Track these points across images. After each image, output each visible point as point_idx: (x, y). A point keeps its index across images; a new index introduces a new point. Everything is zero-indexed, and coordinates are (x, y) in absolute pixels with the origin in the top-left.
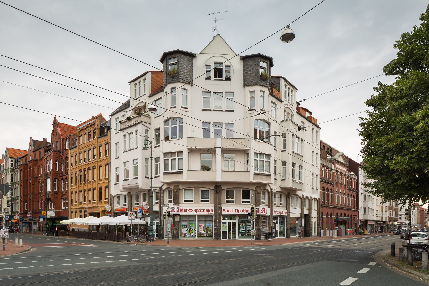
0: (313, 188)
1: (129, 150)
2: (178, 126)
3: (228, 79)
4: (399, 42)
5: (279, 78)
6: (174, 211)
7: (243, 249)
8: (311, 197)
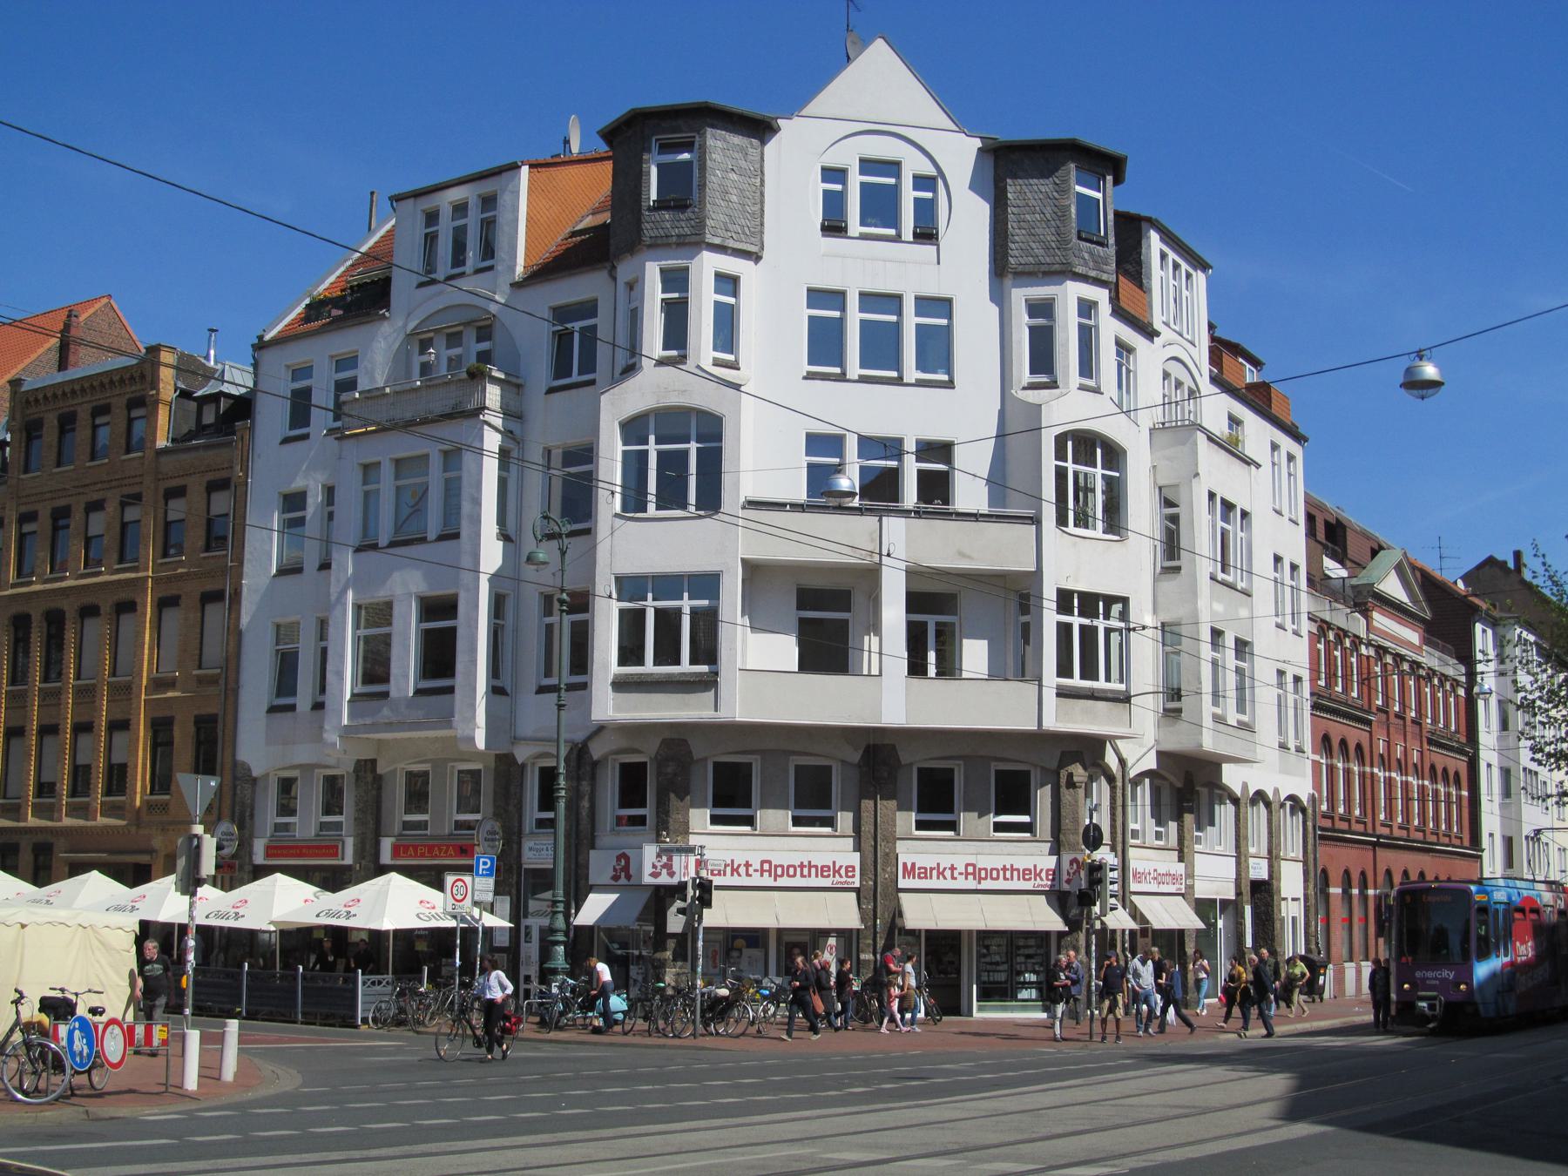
6: (671, 874)
8: (1276, 791)
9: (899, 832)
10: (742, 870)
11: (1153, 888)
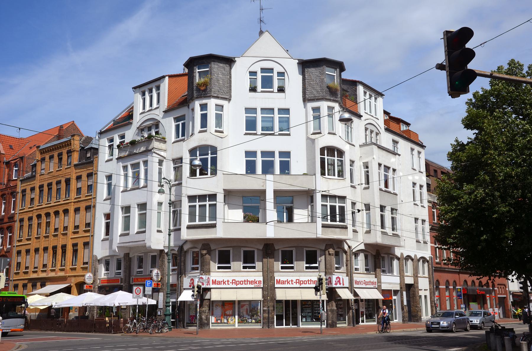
0: (418, 241)
1: (131, 190)
2: (209, 156)
3: (281, 90)
4: (471, 100)
5: (354, 83)
7: (308, 339)
9: (275, 270)
10: (226, 283)
11: (364, 286)
